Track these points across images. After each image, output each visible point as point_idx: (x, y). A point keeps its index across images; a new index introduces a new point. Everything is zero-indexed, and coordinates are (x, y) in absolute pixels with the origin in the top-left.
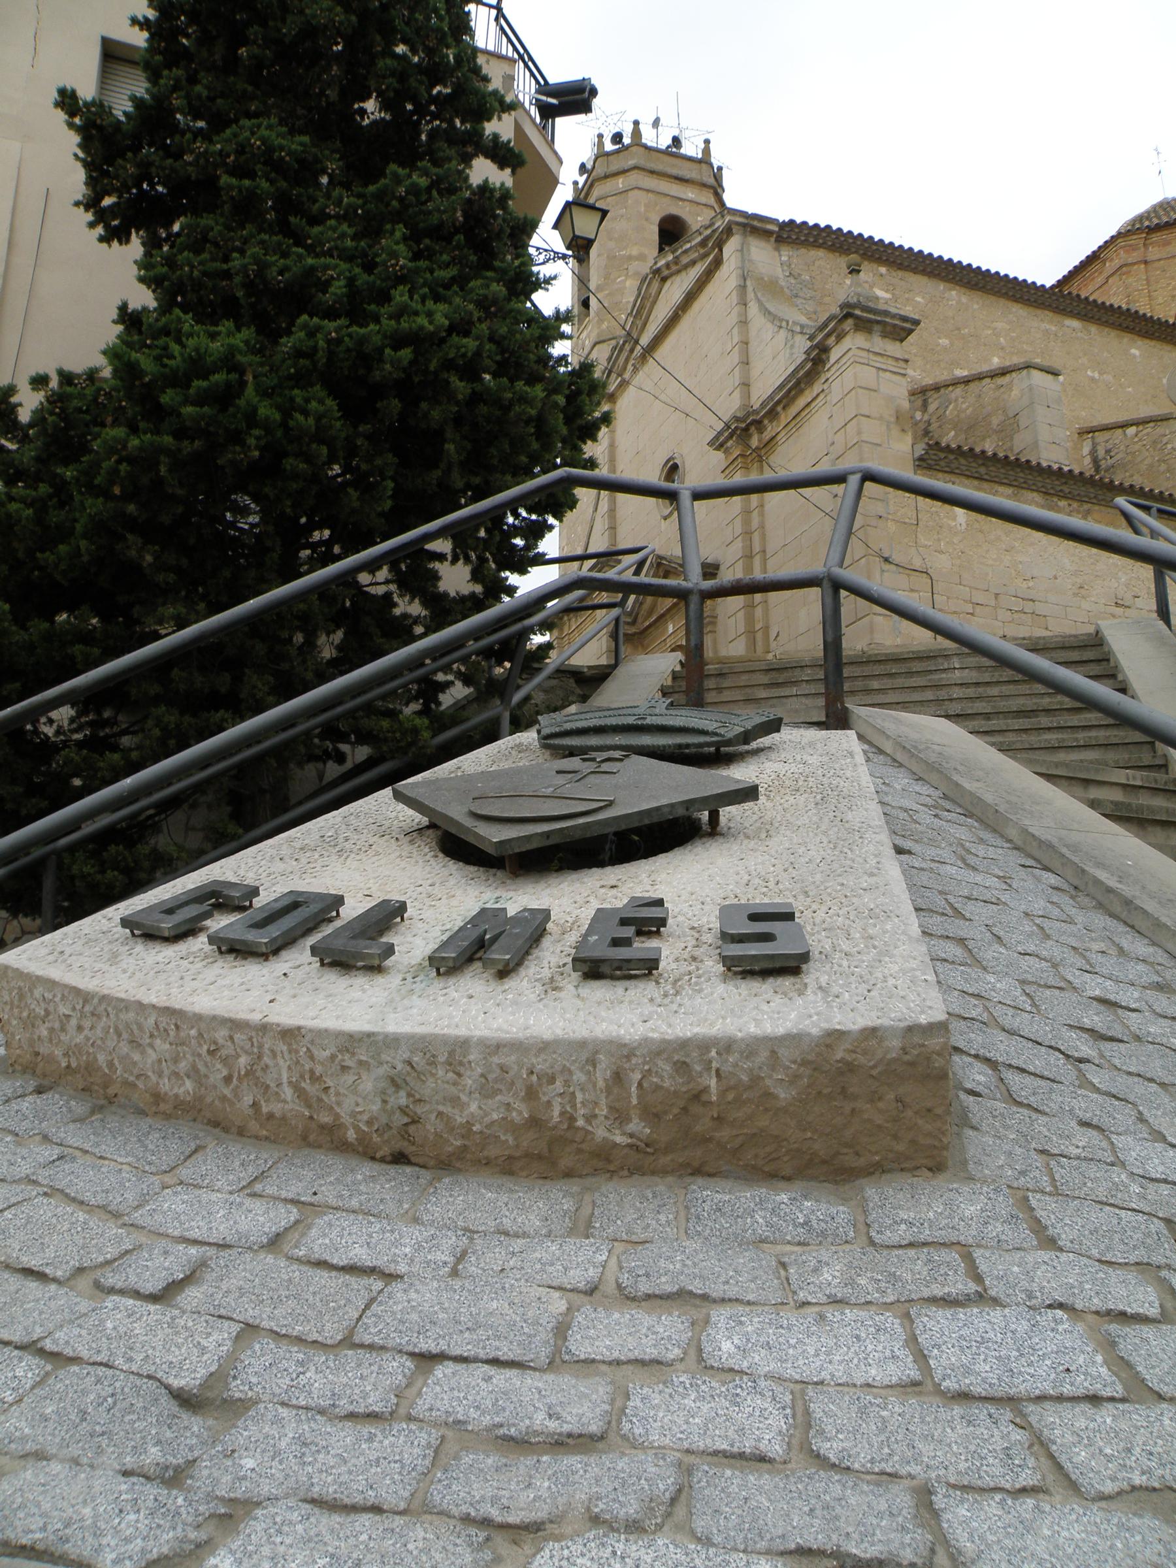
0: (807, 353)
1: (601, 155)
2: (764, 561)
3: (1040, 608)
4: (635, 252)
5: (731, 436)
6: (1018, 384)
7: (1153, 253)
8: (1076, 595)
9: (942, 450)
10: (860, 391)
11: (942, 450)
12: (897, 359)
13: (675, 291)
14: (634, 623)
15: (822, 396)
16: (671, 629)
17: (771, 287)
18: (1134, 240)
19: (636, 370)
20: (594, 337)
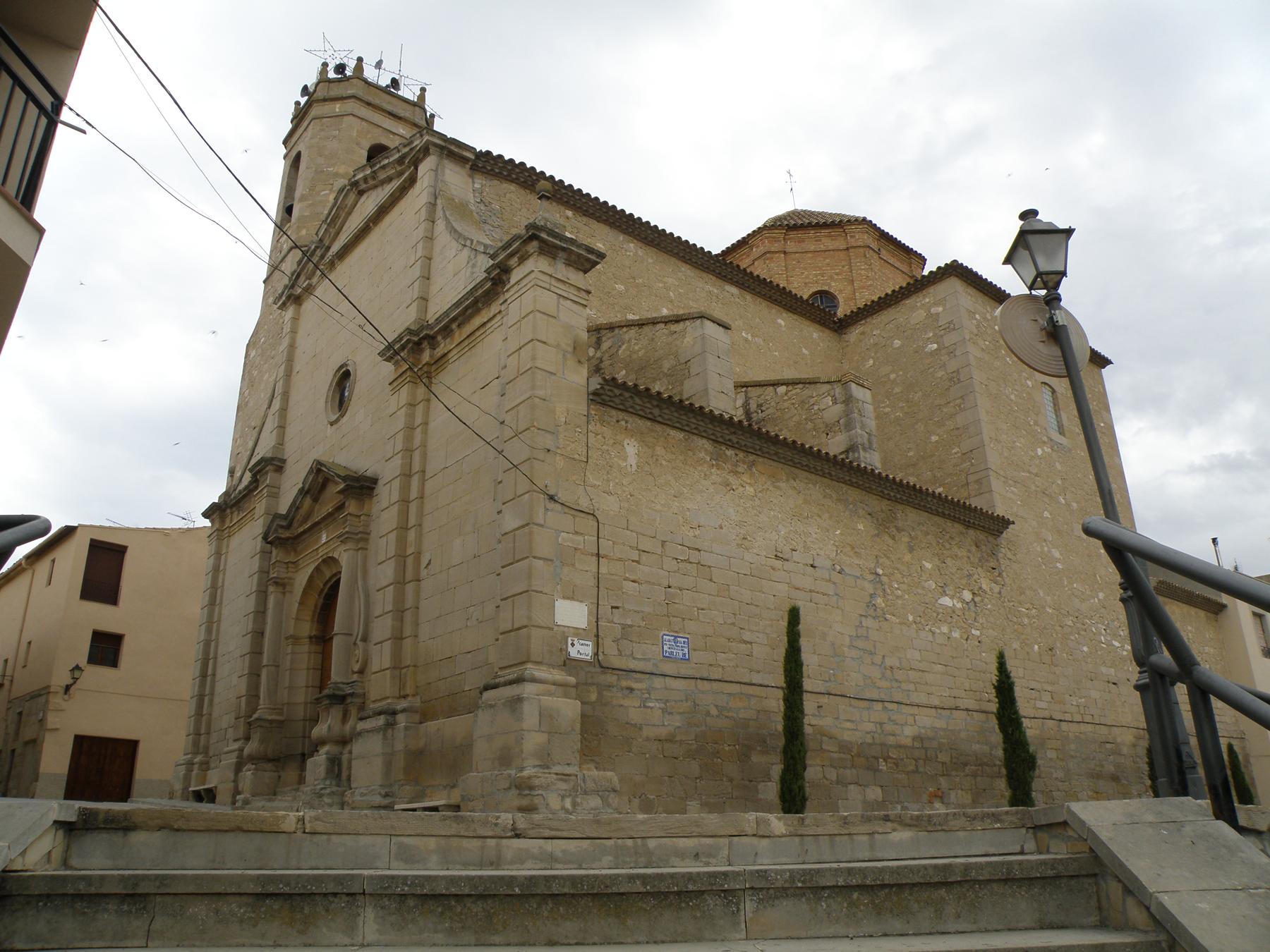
0: (488, 271)
1: (323, 79)
3: (706, 558)
6: (692, 331)
7: (791, 246)
8: (739, 546)
9: (618, 386)
10: (538, 315)
11: (618, 386)
12: (579, 289)
13: (369, 204)
15: (499, 317)
16: (324, 539)
17: (461, 209)
18: (778, 234)
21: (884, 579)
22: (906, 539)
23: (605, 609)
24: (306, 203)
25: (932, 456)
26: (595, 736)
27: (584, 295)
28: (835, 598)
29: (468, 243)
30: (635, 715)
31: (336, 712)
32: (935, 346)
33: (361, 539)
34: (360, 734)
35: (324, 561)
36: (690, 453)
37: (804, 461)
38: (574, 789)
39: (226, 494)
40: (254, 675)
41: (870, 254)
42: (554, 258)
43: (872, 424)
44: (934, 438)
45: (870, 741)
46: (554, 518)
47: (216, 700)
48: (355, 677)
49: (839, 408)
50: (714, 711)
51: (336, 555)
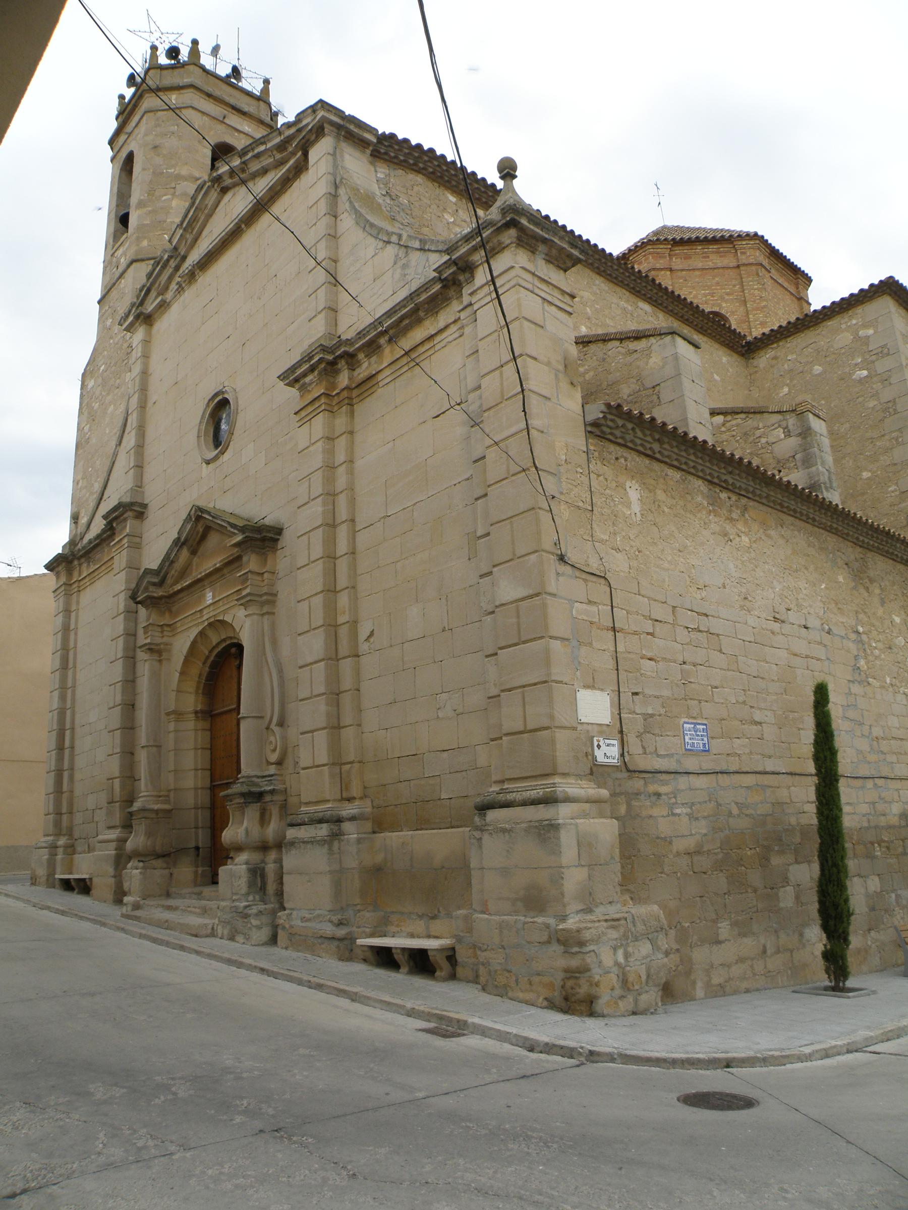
1: (153, 66)
2: (353, 533)
3: (716, 625)
4: (184, 171)
5: (312, 369)
7: (677, 263)
10: (526, 323)
12: (563, 292)
13: (238, 203)
14: (161, 584)
15: (453, 328)
18: (663, 249)
19: (180, 289)
20: (130, 255)
21: (864, 637)
22: (877, 591)
23: (626, 697)
24: (145, 210)
25: (863, 494)
26: (635, 860)
27: (567, 299)
28: (826, 663)
29: (394, 239)
30: (664, 827)
31: (252, 812)
32: (865, 373)
33: (265, 602)
34: (292, 844)
35: (210, 624)
36: (689, 498)
37: (792, 504)
38: (625, 936)
39: (72, 543)
40: (128, 753)
41: (762, 272)
42: (533, 253)
43: (829, 459)
44: (866, 475)
45: (866, 824)
46: (561, 583)
47: (78, 776)
48: (272, 770)
49: (794, 442)
50: (735, 811)
51: (228, 618)
